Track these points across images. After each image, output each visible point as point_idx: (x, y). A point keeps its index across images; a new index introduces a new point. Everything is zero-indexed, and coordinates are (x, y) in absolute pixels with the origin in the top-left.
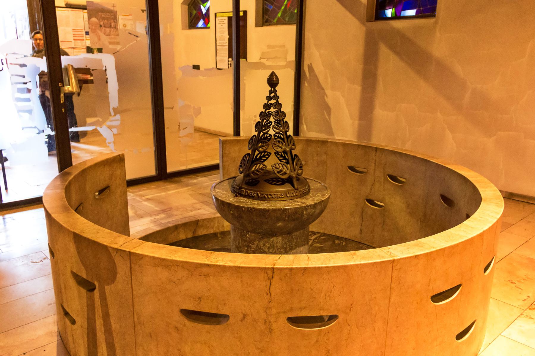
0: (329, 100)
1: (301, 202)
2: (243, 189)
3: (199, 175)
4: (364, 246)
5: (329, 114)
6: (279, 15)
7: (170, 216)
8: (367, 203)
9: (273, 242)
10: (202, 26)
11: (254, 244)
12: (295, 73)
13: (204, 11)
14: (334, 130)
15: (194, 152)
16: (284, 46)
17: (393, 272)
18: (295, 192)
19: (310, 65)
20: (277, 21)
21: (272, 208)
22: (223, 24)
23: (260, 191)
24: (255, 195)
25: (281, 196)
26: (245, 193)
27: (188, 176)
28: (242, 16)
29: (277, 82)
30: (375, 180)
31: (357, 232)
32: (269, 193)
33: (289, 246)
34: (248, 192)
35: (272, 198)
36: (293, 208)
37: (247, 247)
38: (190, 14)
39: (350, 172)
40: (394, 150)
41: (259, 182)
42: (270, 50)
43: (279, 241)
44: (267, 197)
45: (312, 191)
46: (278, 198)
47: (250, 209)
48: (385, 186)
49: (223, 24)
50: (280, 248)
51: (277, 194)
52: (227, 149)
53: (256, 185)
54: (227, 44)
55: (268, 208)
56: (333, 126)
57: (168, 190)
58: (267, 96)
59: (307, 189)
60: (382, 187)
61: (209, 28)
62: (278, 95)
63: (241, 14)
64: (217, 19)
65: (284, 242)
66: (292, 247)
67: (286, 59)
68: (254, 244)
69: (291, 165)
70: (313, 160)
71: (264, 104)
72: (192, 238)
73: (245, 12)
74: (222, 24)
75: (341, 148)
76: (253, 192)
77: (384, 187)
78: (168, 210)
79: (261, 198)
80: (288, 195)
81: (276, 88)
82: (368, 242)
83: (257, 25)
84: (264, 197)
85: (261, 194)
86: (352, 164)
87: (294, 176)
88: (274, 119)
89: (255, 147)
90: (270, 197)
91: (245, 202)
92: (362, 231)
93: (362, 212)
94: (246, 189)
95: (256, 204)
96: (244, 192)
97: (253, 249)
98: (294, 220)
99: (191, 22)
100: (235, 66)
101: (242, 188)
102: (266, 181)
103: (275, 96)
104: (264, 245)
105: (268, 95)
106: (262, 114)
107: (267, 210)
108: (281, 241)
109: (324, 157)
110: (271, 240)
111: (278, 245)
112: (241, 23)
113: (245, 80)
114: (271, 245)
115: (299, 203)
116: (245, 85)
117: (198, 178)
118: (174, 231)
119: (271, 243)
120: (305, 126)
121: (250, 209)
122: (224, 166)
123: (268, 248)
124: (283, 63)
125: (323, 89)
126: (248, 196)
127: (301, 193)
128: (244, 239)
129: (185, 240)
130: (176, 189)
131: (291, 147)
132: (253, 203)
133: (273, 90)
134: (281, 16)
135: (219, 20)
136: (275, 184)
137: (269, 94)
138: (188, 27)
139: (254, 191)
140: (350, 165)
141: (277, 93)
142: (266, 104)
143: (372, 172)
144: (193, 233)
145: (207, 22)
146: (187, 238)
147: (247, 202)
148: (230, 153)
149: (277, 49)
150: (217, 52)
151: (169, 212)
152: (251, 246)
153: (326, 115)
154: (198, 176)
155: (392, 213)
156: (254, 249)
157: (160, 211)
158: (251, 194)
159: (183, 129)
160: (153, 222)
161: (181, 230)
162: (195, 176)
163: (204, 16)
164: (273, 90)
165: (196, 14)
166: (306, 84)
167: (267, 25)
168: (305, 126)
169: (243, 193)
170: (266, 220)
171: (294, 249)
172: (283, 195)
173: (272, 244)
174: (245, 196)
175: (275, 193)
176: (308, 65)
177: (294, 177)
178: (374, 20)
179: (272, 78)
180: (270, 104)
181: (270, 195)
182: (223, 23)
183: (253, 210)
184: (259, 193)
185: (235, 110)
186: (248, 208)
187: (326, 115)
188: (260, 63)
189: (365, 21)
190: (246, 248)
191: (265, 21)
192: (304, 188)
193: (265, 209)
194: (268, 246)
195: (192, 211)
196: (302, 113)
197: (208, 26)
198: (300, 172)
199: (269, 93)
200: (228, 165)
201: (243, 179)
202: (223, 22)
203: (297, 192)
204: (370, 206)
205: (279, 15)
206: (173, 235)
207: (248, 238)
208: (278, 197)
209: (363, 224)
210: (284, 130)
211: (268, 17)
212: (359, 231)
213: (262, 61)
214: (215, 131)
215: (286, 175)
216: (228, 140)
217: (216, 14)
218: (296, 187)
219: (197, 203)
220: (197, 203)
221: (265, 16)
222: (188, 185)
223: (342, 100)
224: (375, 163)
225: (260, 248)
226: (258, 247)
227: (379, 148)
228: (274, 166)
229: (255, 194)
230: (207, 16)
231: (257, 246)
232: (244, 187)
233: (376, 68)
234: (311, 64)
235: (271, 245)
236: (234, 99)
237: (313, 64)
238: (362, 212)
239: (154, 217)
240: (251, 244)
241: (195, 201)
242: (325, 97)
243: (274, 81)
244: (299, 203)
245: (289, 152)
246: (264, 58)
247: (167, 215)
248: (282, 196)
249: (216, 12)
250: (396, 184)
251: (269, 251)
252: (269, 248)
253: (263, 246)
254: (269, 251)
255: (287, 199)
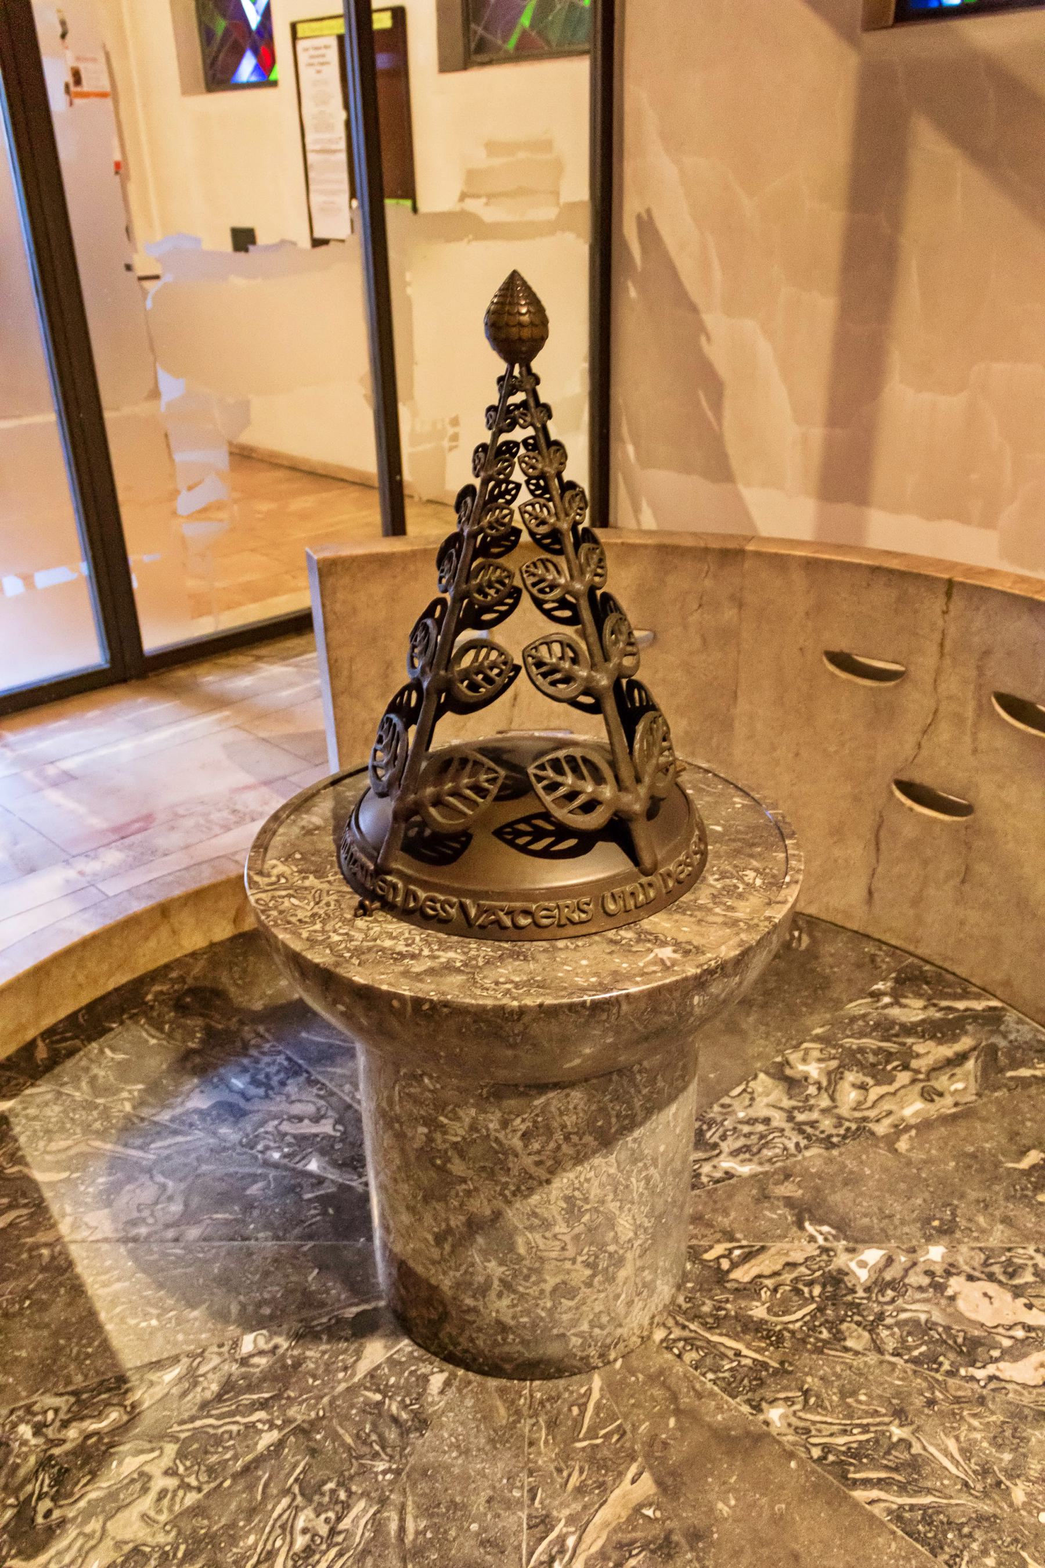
0: (717, 353)
1: (677, 945)
2: (395, 880)
3: (263, 651)
4: (880, 949)
5: (717, 405)
6: (525, 21)
7: (145, 856)
8: (898, 794)
9: (543, 1112)
10: (254, 79)
11: (458, 1119)
12: (592, 248)
13: (254, 20)
14: (735, 463)
15: (252, 550)
16: (546, 145)
17: (873, 842)
18: (641, 885)
19: (645, 217)
20: (517, 48)
21: (539, 1001)
22: (322, 64)
23: (475, 895)
24: (453, 911)
25: (576, 916)
26: (406, 900)
27: (223, 661)
28: (384, 32)
29: (536, 332)
30: (936, 712)
31: (856, 893)
32: (518, 905)
33: (618, 1116)
34: (416, 898)
35: (534, 928)
36: (642, 992)
37: (425, 1125)
38: (207, 34)
39: (833, 674)
40: (1030, 595)
41: (470, 837)
42: (497, 162)
43: (571, 1107)
44: (507, 921)
45: (718, 856)
46: (560, 926)
47: (426, 1007)
48: (982, 736)
49: (322, 64)
50: (576, 1133)
51: (558, 907)
52: (340, 596)
53: (457, 854)
54: (342, 145)
55: (515, 1003)
56: (731, 451)
57: (146, 727)
58: (491, 408)
59: (696, 853)
60: (967, 739)
61: (274, 84)
62: (543, 400)
63: (382, 22)
64: (301, 45)
65: (594, 1107)
66: (632, 1117)
67: (556, 194)
68: (458, 1119)
69: (611, 720)
70: (685, 627)
71: (476, 451)
72: (233, 939)
73: (399, 14)
74: (319, 68)
75: (799, 578)
76: (442, 898)
77: (974, 734)
78: (137, 825)
79: (482, 927)
80: (611, 907)
81: (536, 365)
82: (898, 937)
83: (446, 65)
84: (498, 922)
85: (482, 911)
86: (842, 644)
87: (637, 807)
88: (525, 473)
89: (442, 673)
90: (523, 921)
91: (402, 956)
92: (876, 895)
93: (880, 826)
94: (407, 879)
95: (458, 971)
96: (401, 893)
97: (456, 1135)
98: (647, 1039)
99: (213, 64)
100: (369, 231)
101: (389, 873)
102: (499, 833)
103: (532, 403)
104: (505, 1124)
105: (486, 437)
106: (469, 500)
107: (512, 1012)
108: (581, 1105)
109: (729, 614)
110: (536, 1103)
111: (570, 1120)
112: (382, 61)
113: (409, 284)
114: (535, 1122)
115: (666, 953)
116: (408, 300)
117: (260, 665)
118: (155, 928)
119: (537, 1115)
120: (630, 449)
121: (426, 1007)
122: (336, 661)
123: (523, 1135)
124: (548, 213)
125: (694, 309)
126: (418, 914)
127: (671, 884)
128: (412, 1090)
129: (204, 951)
130: (176, 722)
131: (620, 664)
132: (445, 956)
133: (516, 372)
134: (532, 26)
135: (306, 50)
136: (546, 854)
137: (498, 396)
138: (203, 85)
139: (442, 889)
140: (835, 648)
141: (538, 388)
142: (484, 447)
143: (929, 679)
144: (234, 921)
145: (266, 63)
146: (212, 945)
147: (413, 956)
148: (355, 611)
149: (522, 155)
150: (311, 175)
151: (139, 837)
152: (443, 1126)
153: (704, 403)
154: (259, 658)
155: (1006, 843)
156: (459, 1139)
157: (103, 832)
158: (434, 909)
159: (190, 488)
160: (74, 892)
161: (185, 919)
162: (250, 659)
163: (256, 37)
164: (516, 372)
165: (227, 32)
166: (633, 293)
167: (483, 64)
168: (630, 449)
169: (395, 897)
170: (510, 1053)
171: (641, 1124)
172: (585, 907)
173: (540, 1119)
174: (405, 914)
175: (546, 904)
176: (639, 217)
177: (635, 813)
178: (891, 21)
179: (510, 314)
180: (506, 443)
181: (527, 913)
182: (321, 60)
183: (445, 1010)
184: (468, 902)
185: (377, 402)
186: (417, 1002)
187: (704, 403)
188: (463, 214)
189: (859, 31)
190: (425, 1130)
191: (473, 46)
192: (682, 858)
193: (502, 1008)
194: (523, 1127)
195: (227, 829)
196: (621, 401)
197: (273, 77)
198: (627, 662)
199: (500, 390)
200: (351, 660)
201: (393, 828)
202: (323, 56)
203: (650, 885)
204: (911, 810)
205: (525, 21)
206: (152, 943)
207: (430, 1091)
208: (563, 921)
209: (879, 870)
210: (582, 581)
211: (486, 28)
212: (864, 893)
213: (471, 205)
214: (326, 466)
215: (600, 809)
216: (340, 558)
217: (294, 27)
218: (647, 860)
219: (248, 788)
220: (248, 788)
221: (473, 26)
222: (218, 702)
223: (764, 349)
224: (942, 645)
225: (488, 1136)
226: (477, 1131)
227: (963, 584)
228: (529, 508)
229: (451, 907)
230: (266, 36)
231: (473, 1128)
232: (400, 867)
233: (897, 225)
234: (649, 211)
235: (535, 1122)
236: (373, 360)
237: (656, 215)
238: (880, 826)
239: (82, 865)
240: (446, 1117)
241: (244, 778)
242: (703, 339)
243: (521, 325)
244: (666, 953)
245: (611, 693)
246: (477, 196)
247: (131, 853)
248: (584, 912)
249: (294, 19)
250: (1036, 737)
251: (526, 1146)
252: (526, 1136)
253: (498, 1127)
254: (526, 1146)
255: (604, 922)
